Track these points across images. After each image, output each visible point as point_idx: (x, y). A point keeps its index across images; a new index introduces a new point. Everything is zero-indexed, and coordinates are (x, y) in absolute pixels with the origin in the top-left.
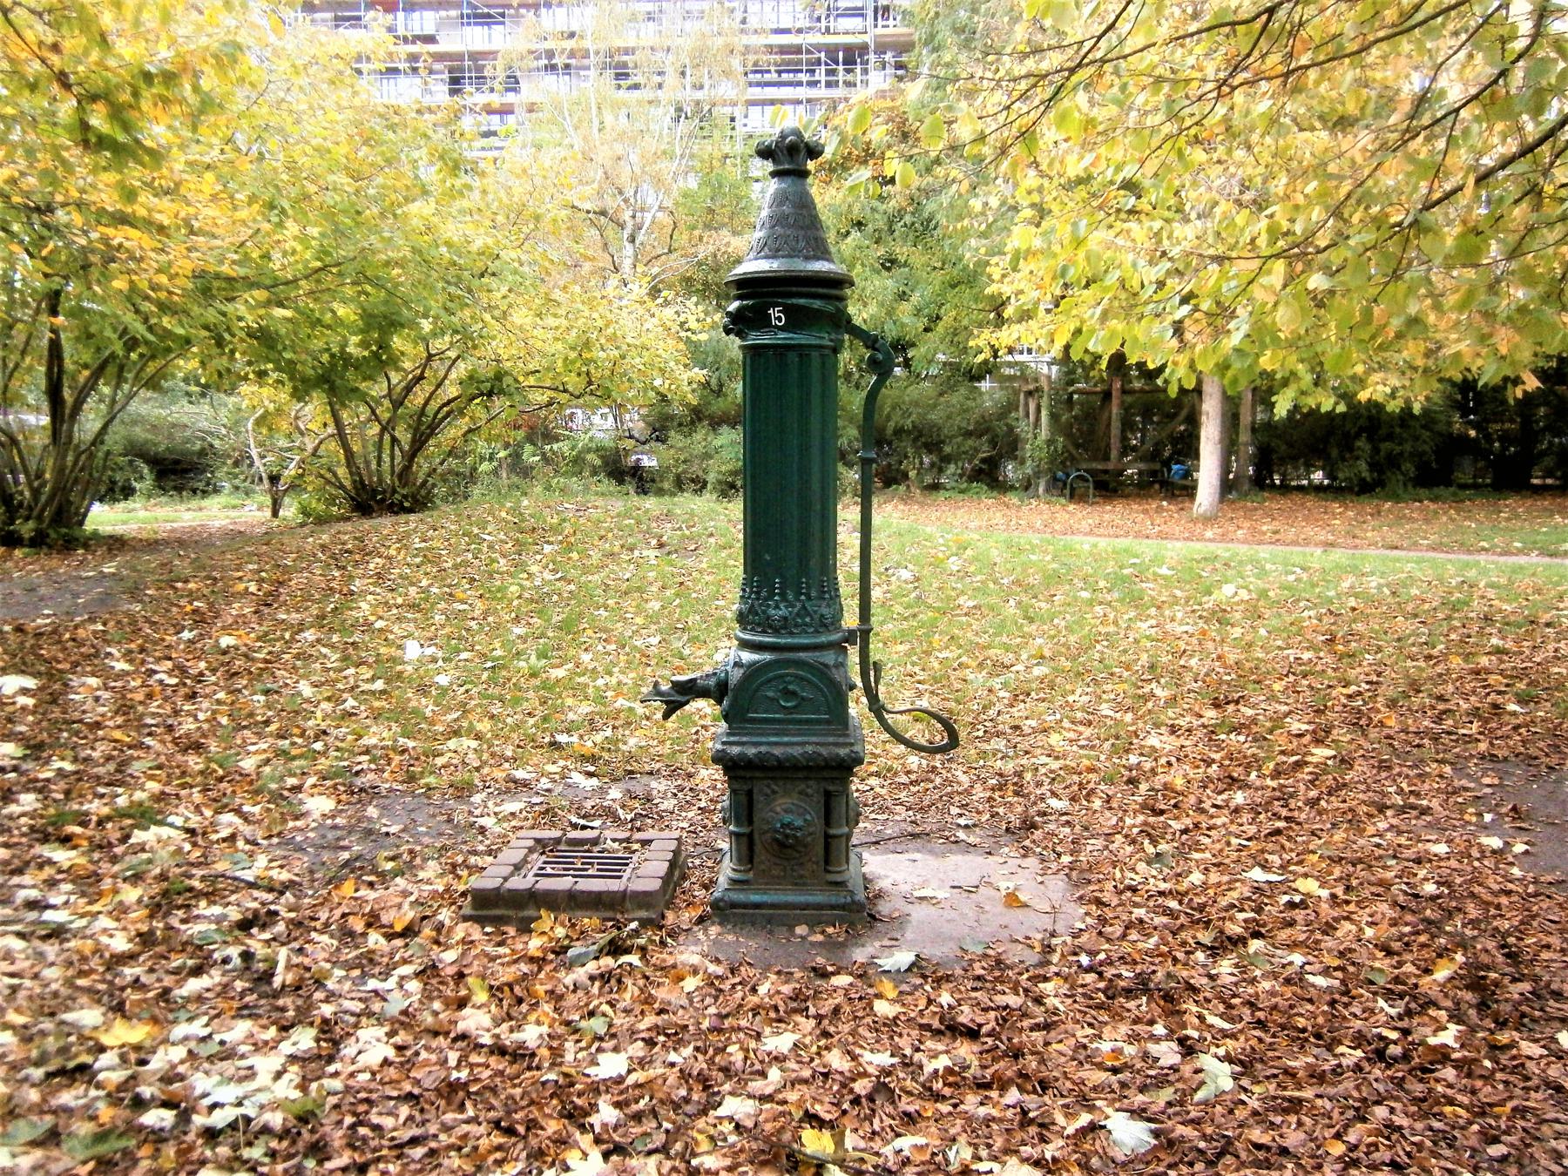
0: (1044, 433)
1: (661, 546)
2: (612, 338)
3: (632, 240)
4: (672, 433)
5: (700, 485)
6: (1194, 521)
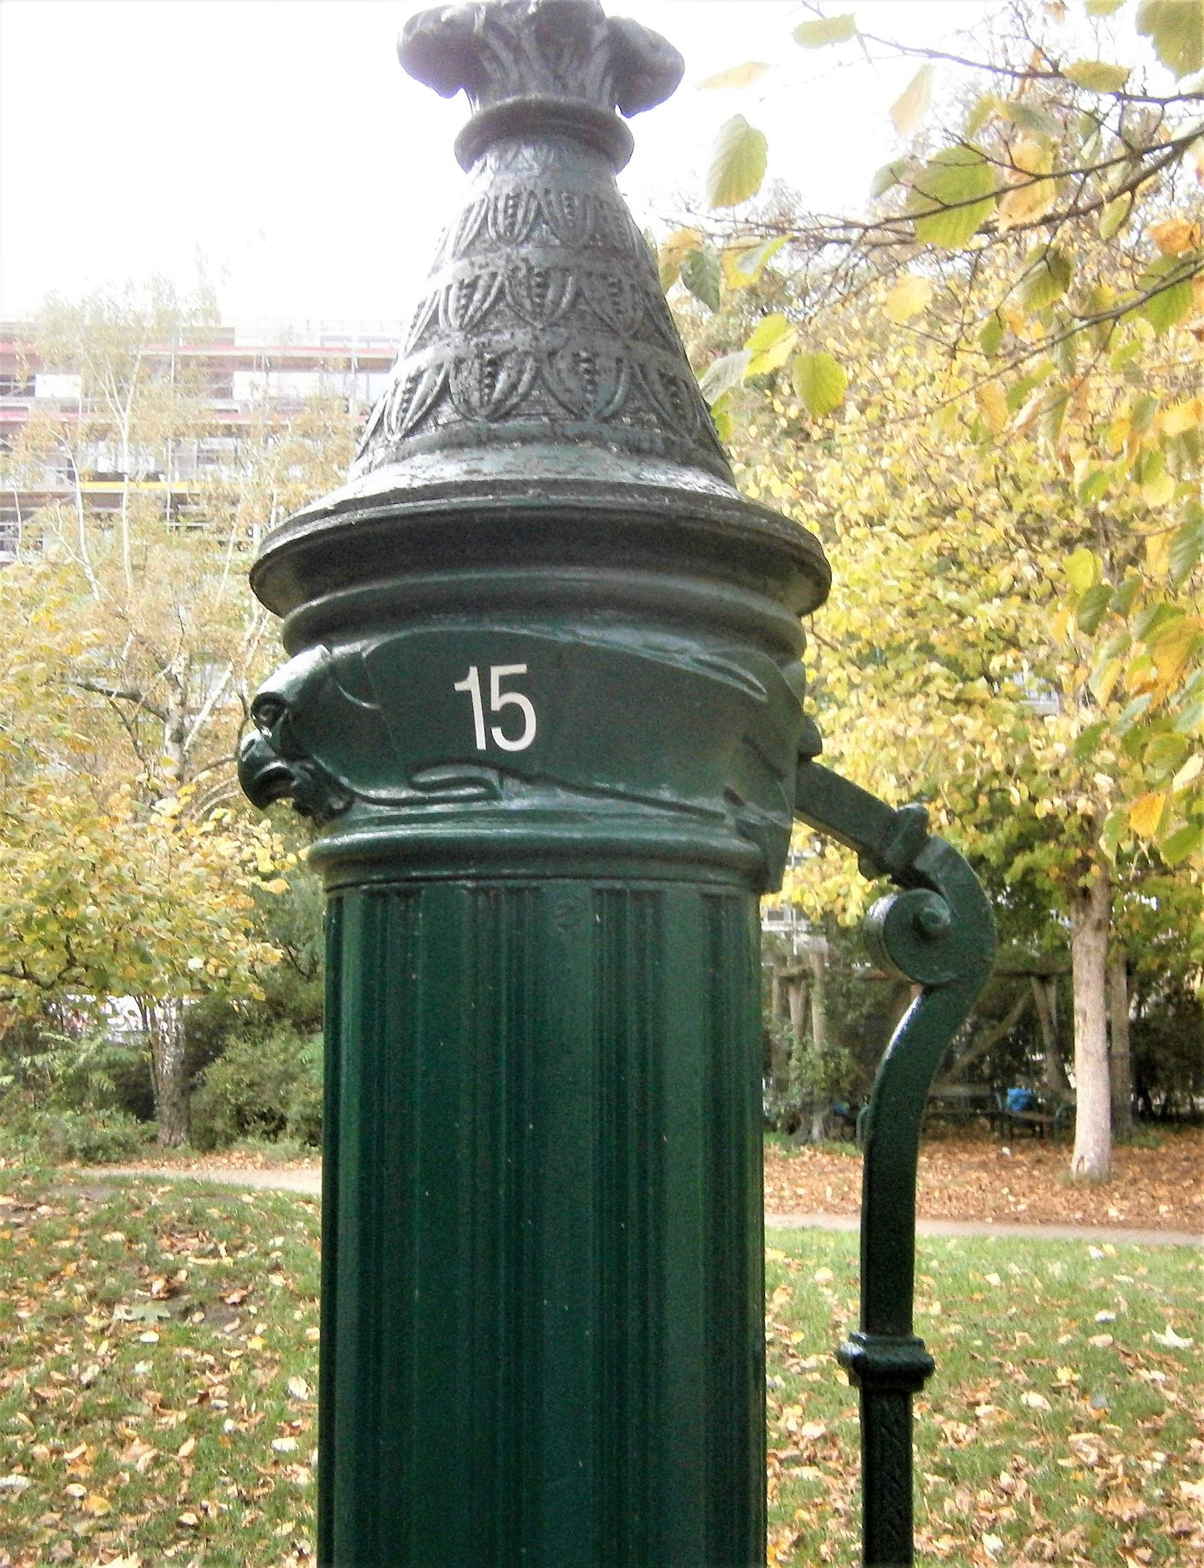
0: (817, 1040)
1: (173, 1292)
2: (115, 883)
3: (179, 737)
4: (232, 1039)
5: (274, 1125)
6: (1070, 1185)
